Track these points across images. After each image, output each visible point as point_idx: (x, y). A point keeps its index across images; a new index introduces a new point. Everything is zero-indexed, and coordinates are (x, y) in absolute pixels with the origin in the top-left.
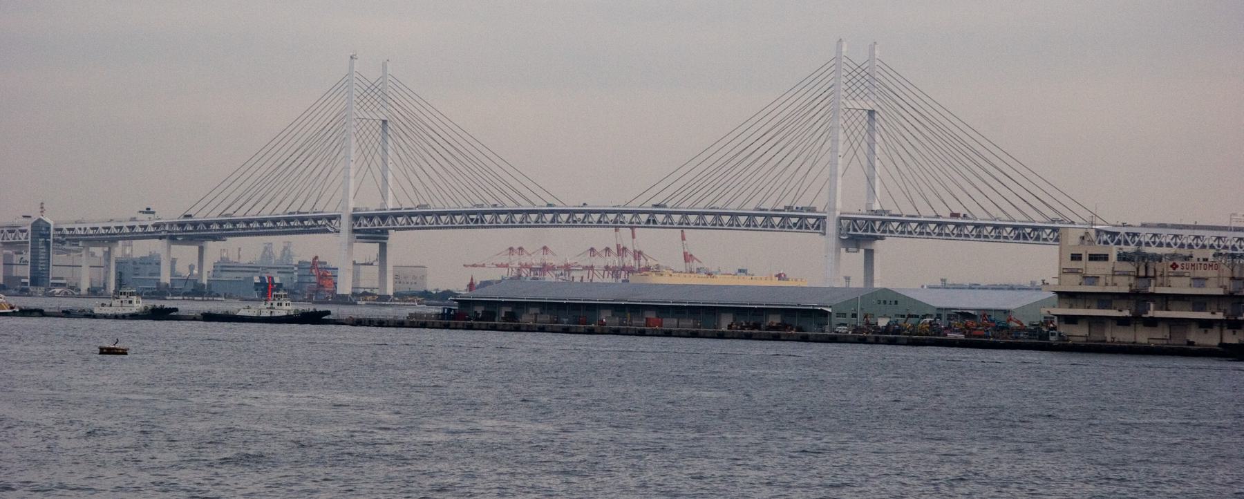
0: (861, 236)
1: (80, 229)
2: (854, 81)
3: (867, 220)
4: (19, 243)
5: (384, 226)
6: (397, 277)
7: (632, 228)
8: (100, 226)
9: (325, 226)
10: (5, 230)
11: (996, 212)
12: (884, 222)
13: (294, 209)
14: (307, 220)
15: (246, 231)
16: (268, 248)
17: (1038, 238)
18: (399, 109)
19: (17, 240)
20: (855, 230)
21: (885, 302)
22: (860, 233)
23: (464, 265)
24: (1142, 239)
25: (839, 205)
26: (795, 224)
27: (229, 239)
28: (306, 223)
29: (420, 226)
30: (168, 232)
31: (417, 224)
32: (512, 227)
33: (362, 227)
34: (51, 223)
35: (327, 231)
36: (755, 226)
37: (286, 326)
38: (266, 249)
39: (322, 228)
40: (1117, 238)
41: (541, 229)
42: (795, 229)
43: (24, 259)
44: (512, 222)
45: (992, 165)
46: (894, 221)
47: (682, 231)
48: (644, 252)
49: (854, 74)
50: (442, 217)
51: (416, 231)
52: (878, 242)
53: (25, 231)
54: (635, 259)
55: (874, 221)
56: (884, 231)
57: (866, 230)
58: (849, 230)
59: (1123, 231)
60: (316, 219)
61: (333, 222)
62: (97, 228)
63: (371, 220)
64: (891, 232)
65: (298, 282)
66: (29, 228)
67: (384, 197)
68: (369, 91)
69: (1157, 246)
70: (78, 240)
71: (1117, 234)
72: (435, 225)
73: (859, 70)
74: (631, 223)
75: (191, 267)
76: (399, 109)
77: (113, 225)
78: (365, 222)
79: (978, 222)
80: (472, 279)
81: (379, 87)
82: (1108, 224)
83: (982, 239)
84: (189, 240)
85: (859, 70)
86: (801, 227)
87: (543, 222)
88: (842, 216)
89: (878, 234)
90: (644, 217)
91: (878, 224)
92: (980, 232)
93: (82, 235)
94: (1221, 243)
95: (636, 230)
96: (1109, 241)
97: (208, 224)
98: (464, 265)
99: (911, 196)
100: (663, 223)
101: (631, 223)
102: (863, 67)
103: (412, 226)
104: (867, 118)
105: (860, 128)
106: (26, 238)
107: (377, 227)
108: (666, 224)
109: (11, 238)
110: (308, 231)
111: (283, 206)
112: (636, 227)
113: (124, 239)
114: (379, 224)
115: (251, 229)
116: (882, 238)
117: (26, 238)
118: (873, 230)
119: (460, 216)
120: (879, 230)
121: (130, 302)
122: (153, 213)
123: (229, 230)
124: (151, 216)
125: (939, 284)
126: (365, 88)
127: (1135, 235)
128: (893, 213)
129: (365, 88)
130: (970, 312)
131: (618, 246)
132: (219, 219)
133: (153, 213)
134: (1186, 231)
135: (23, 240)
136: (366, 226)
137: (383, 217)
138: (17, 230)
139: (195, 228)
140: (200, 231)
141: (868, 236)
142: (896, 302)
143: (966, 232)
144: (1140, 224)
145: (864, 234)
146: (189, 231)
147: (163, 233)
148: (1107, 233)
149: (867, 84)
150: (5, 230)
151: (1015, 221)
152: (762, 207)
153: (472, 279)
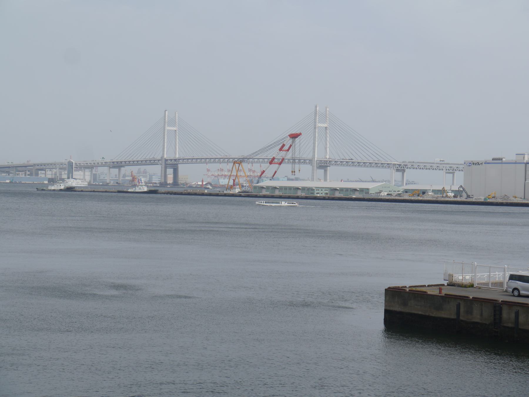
0: (323, 166)
1: (82, 164)
2: (322, 119)
3: (325, 161)
4: (64, 168)
5: (175, 163)
6: (395, 181)
7: (252, 163)
8: (88, 163)
9: (157, 163)
10: (60, 164)
11: (376, 159)
12: (330, 161)
13: (151, 157)
14: (156, 160)
15: (145, 164)
16: (139, 169)
17: (383, 167)
18: (339, 128)
19: (63, 167)
20: (321, 164)
21: (384, 187)
22: (323, 165)
23: (204, 175)
24: (408, 167)
25: (165, 157)
26: (303, 162)
27: (126, 167)
28: (151, 162)
29: (187, 162)
30: (109, 164)
31: (185, 162)
32: (215, 163)
33: (169, 163)
34: (74, 162)
35: (158, 164)
36: (290, 162)
37: (142, 194)
38: (139, 170)
39: (156, 163)
40: (401, 166)
41: (215, 164)
42: (303, 164)
43: (66, 173)
44: (220, 161)
45: (363, 144)
46: (333, 161)
47: (260, 164)
48: (291, 171)
49: (321, 116)
50: (184, 160)
51: (185, 164)
52: (328, 167)
53: (66, 164)
54: (253, 173)
55: (327, 161)
56: (330, 164)
57: (325, 164)
58: (319, 164)
59: (402, 164)
60: (154, 161)
61: (160, 161)
62: (87, 163)
63: (171, 161)
64: (332, 164)
65: (149, 180)
66: (67, 163)
67: (175, 154)
68: (169, 122)
69: (413, 169)
70: (82, 167)
71: (401, 165)
72: (191, 162)
73: (322, 115)
74: (252, 162)
75: (116, 175)
76: (339, 128)
77: (92, 162)
78: (170, 161)
79: (359, 161)
80: (203, 179)
81: (174, 120)
82: (398, 162)
83: (360, 166)
84: (114, 167)
85: (322, 115)
86: (304, 163)
87: (229, 161)
88: (317, 159)
89: (328, 165)
90: (308, 161)
91: (328, 162)
92: (359, 164)
93: (83, 166)
94: (458, 169)
95: (253, 164)
96: (398, 167)
97: (121, 162)
98: (204, 175)
99: (304, 154)
100: (262, 162)
101: (252, 162)
102: (324, 113)
103: (184, 163)
104: (325, 129)
105: (323, 135)
106: (66, 166)
107: (173, 163)
108: (263, 162)
109: (61, 166)
110: (152, 164)
111: (132, 158)
112: (208, 163)
113: (96, 167)
114: (174, 162)
115: (135, 163)
116: (329, 166)
117: (66, 166)
118: (327, 164)
119: (199, 160)
120: (328, 164)
121: (60, 185)
122: (104, 159)
123: (128, 164)
124: (104, 159)
125: (347, 180)
126: (171, 119)
127: (406, 165)
128: (332, 158)
129: (170, 120)
130: (357, 189)
131: (221, 168)
132: (125, 160)
133: (104, 159)
134: (461, 165)
135: (65, 167)
136: (170, 163)
137: (175, 160)
138: (63, 164)
139: (117, 164)
140: (119, 164)
141: (325, 166)
142: (389, 187)
143: (355, 165)
144: (402, 162)
145: (324, 165)
146: (116, 164)
147: (108, 165)
148: (398, 165)
149: (325, 119)
150: (60, 164)
151: (370, 161)
152: (302, 157)
153: (203, 179)
